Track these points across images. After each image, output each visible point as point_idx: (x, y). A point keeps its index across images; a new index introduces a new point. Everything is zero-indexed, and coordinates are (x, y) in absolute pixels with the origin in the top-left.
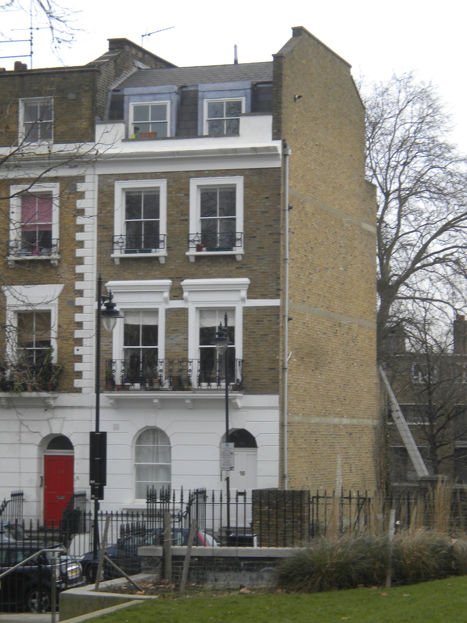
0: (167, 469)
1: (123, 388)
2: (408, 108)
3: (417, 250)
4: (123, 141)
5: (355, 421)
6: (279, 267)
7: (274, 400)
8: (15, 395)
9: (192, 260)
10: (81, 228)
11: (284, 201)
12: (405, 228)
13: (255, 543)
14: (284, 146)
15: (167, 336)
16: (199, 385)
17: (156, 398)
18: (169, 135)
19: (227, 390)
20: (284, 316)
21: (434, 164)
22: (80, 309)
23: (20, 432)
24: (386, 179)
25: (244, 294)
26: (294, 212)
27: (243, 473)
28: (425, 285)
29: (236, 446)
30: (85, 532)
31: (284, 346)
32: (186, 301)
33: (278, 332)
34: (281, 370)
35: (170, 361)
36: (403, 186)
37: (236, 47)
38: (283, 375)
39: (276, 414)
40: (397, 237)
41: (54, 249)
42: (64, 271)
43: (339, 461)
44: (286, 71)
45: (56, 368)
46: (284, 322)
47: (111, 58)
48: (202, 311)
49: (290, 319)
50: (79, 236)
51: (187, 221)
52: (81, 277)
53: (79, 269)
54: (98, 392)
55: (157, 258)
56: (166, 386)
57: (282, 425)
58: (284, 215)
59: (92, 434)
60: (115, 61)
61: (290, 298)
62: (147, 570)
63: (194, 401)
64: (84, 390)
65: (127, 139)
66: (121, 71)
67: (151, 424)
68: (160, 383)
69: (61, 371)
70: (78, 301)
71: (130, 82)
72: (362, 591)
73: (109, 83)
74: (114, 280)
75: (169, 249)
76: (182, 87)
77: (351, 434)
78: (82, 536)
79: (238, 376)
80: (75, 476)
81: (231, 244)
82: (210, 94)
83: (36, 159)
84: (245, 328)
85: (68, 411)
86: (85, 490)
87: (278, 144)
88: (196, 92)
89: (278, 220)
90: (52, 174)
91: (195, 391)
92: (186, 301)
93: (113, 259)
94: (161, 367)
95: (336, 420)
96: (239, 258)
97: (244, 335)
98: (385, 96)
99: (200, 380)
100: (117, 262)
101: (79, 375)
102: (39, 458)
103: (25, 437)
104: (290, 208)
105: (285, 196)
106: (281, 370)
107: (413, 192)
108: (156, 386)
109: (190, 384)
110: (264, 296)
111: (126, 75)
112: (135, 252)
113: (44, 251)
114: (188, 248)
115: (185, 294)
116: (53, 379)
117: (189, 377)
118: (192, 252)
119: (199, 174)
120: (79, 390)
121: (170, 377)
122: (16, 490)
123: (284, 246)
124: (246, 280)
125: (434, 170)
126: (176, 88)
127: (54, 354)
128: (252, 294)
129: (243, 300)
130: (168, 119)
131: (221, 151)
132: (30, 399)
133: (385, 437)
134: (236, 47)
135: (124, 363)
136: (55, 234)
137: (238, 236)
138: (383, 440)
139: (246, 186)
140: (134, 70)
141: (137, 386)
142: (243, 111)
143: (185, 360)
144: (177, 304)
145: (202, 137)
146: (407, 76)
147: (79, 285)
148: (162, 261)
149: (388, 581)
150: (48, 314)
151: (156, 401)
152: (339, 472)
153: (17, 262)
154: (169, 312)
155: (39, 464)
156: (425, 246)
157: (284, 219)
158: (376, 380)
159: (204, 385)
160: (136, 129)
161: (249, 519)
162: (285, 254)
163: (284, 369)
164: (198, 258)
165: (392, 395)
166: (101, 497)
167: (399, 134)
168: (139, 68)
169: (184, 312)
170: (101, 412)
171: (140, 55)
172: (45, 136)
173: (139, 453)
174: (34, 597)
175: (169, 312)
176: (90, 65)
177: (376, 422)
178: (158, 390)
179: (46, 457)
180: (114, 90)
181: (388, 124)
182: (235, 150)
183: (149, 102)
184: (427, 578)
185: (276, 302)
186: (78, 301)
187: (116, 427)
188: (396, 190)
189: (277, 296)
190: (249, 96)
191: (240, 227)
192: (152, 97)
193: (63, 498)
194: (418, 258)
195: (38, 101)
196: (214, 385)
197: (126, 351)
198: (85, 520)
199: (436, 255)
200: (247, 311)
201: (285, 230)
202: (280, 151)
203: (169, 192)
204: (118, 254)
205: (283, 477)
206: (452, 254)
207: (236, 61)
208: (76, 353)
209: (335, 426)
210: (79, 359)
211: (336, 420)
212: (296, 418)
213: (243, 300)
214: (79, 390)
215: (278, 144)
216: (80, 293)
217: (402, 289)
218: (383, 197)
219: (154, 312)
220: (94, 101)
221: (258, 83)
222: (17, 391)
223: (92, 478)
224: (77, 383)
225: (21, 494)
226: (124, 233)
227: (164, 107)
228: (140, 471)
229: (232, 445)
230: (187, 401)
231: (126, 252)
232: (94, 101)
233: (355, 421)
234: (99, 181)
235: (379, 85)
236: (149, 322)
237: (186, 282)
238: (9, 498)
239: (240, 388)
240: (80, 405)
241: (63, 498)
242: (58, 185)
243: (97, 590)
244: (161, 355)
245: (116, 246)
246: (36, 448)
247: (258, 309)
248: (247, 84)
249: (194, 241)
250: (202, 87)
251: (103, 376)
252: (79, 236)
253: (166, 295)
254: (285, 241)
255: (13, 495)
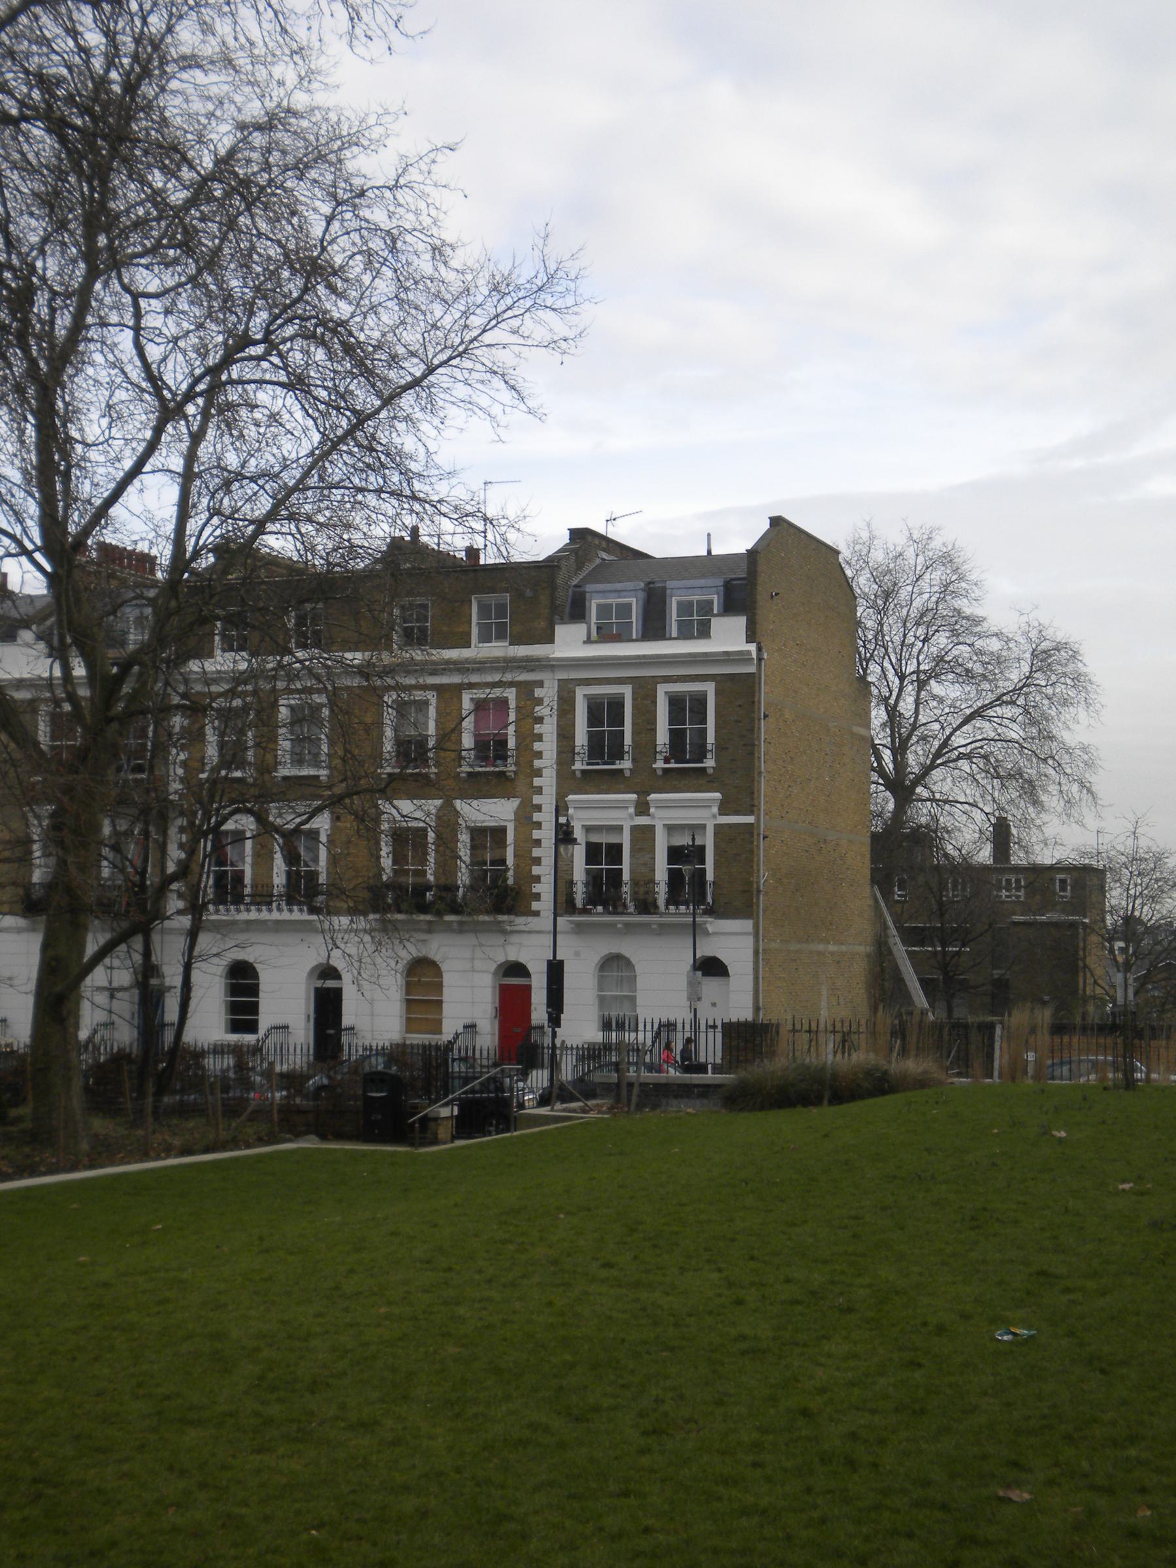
0: (632, 1000)
1: (584, 911)
2: (927, 576)
3: (936, 744)
4: (585, 642)
5: (844, 948)
6: (753, 781)
7: (747, 925)
8: (465, 918)
9: (660, 773)
10: (540, 738)
11: (759, 709)
12: (922, 719)
13: (710, 1071)
14: (759, 649)
15: (632, 856)
16: (667, 908)
17: (620, 922)
18: (634, 637)
19: (694, 914)
20: (759, 835)
21: (961, 639)
22: (538, 825)
23: (473, 959)
24: (901, 660)
25: (715, 810)
26: (770, 720)
27: (714, 1005)
28: (947, 786)
29: (703, 975)
30: (542, 1067)
31: (758, 865)
32: (653, 817)
33: (752, 851)
34: (755, 892)
35: (635, 883)
36: (922, 667)
37: (709, 535)
38: (758, 899)
39: (750, 940)
40: (914, 727)
41: (510, 760)
42: (521, 787)
43: (824, 992)
44: (762, 567)
45: (512, 889)
46: (759, 842)
47: (571, 551)
48: (671, 829)
49: (765, 837)
50: (537, 746)
51: (654, 730)
52: (539, 790)
53: (537, 782)
54: (556, 915)
55: (621, 771)
56: (631, 909)
57: (756, 953)
58: (759, 724)
59: (549, 962)
60: (576, 553)
61: (766, 814)
62: (602, 1097)
63: (662, 926)
64: (542, 914)
65: (589, 641)
66: (583, 564)
67: (615, 950)
68: (625, 906)
69: (517, 893)
70: (536, 817)
71: (593, 577)
72: (799, 1109)
73: (570, 578)
74: (575, 794)
75: (634, 760)
76: (650, 583)
77: (838, 962)
78: (540, 1072)
79: (709, 900)
80: (533, 1007)
81: (701, 755)
82: (679, 592)
83: (492, 662)
84: (716, 846)
85: (525, 936)
86: (502, 824)
87: (752, 648)
88: (664, 589)
89: (752, 730)
90: (508, 677)
91: (661, 915)
92: (653, 817)
93: (574, 771)
94: (625, 889)
95: (821, 947)
96: (710, 771)
97: (715, 854)
98: (899, 561)
99: (668, 903)
100: (578, 774)
101: (537, 897)
102: (494, 987)
103: (478, 964)
104: (766, 716)
105: (759, 702)
106: (755, 892)
107: (934, 674)
108: (620, 909)
109: (656, 907)
110: (737, 813)
111: (589, 567)
112: (598, 764)
113: (499, 762)
114: (655, 761)
115: (652, 810)
116: (509, 901)
117: (655, 899)
118: (660, 764)
119: (667, 679)
120: (537, 914)
121: (633, 899)
122: (469, 1021)
123: (759, 758)
124: (718, 795)
125: (960, 647)
126: (642, 585)
127: (510, 873)
128: (723, 810)
129: (714, 816)
130: (634, 619)
131: (690, 655)
132: (484, 922)
133: (881, 965)
134: (709, 535)
135: (586, 885)
136: (511, 743)
137: (709, 747)
138: (878, 969)
139: (718, 693)
140: (598, 561)
141: (600, 909)
142: (715, 611)
143: (652, 881)
144: (643, 820)
145: (671, 639)
146: (925, 537)
147: (537, 799)
148: (627, 774)
149: (826, 1102)
150: (503, 830)
151: (619, 926)
152: (824, 1004)
153: (469, 774)
154: (634, 829)
155: (494, 992)
156: (949, 738)
157: (759, 728)
158: (870, 902)
159: (672, 908)
160: (599, 628)
161: (719, 1054)
162: (760, 767)
163: (759, 891)
164: (665, 770)
165: (889, 919)
166: (559, 1026)
167: (918, 603)
168: (603, 559)
169: (651, 829)
170: (559, 937)
171: (604, 544)
172: (501, 636)
173: (601, 984)
174: (491, 1125)
175: (634, 829)
176: (550, 559)
177: (869, 949)
178: (622, 913)
179: (501, 986)
180: (576, 586)
181: (904, 594)
182: (706, 654)
183: (613, 600)
184: (862, 1097)
185: (750, 819)
186: (536, 817)
187: (577, 954)
188: (913, 672)
189: (751, 813)
190: (722, 593)
191: (711, 738)
192: (613, 594)
193: (519, 1030)
194: (938, 754)
195: (492, 598)
196: (682, 908)
197: (588, 871)
198: (543, 1054)
199: (961, 750)
200: (719, 829)
201: (760, 741)
202: (754, 656)
203: (634, 699)
204: (578, 766)
205: (757, 1009)
206: (982, 747)
207: (709, 552)
208: (534, 890)
209: (820, 953)
210: (537, 879)
211: (821, 947)
212: (773, 945)
213: (714, 816)
214: (537, 914)
215: (752, 648)
216: (539, 808)
217: (919, 790)
218: (897, 681)
219: (619, 829)
220: (553, 599)
221: (732, 579)
222: (470, 914)
223: (549, 1005)
224: (535, 906)
225: (474, 1026)
226: (586, 743)
227: (630, 605)
228: (602, 1000)
229: (699, 973)
230: (654, 926)
231: (588, 764)
232: (553, 599)
233: (844, 948)
234: (559, 686)
235: (892, 548)
236: (613, 839)
237: (653, 796)
238: (461, 1030)
239: (711, 912)
240: (537, 929)
241: (519, 1030)
242: (514, 690)
243: (552, 1110)
244: (626, 876)
245: (577, 757)
246: (490, 976)
247: (730, 826)
248: (720, 582)
249: (661, 752)
250: (670, 584)
251: (562, 899)
252: (537, 746)
253: (632, 810)
254: (760, 753)
255: (465, 1027)
